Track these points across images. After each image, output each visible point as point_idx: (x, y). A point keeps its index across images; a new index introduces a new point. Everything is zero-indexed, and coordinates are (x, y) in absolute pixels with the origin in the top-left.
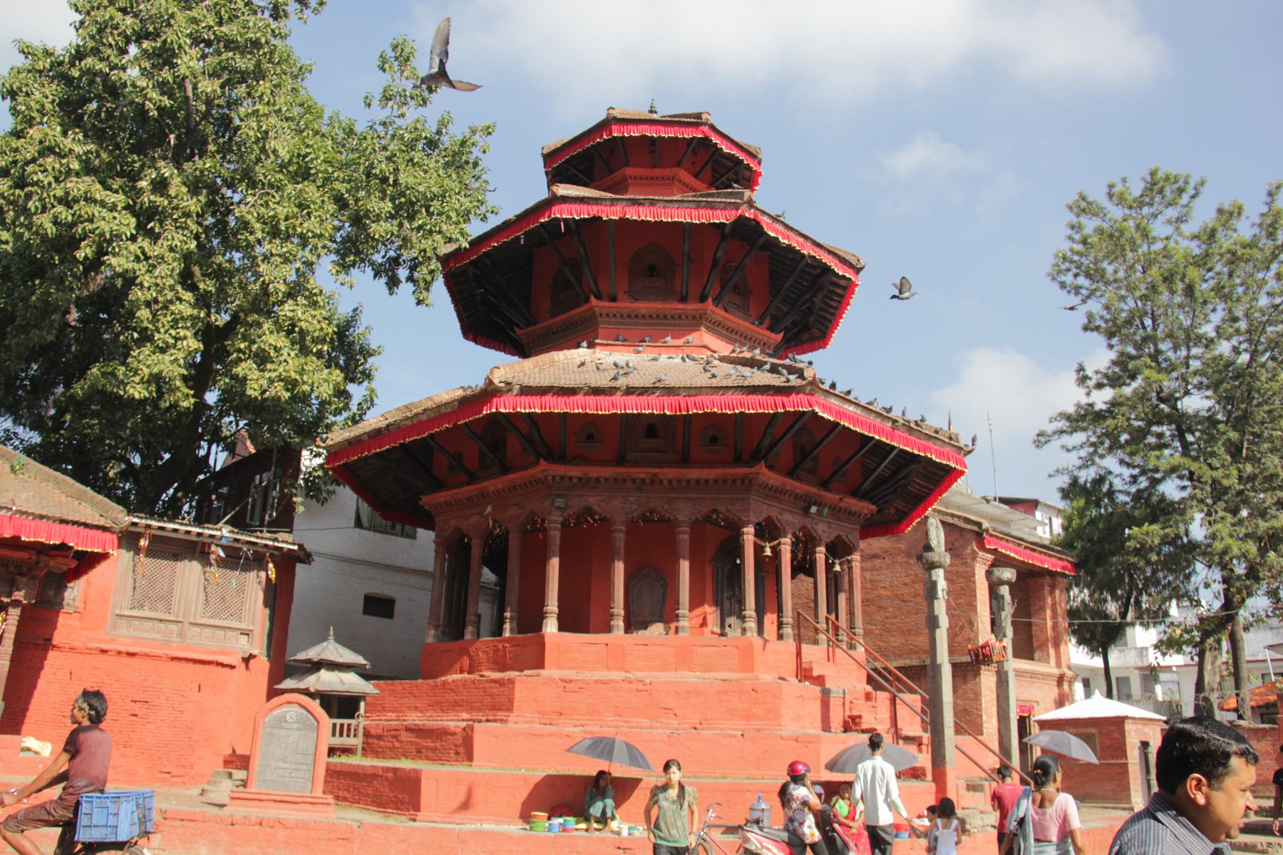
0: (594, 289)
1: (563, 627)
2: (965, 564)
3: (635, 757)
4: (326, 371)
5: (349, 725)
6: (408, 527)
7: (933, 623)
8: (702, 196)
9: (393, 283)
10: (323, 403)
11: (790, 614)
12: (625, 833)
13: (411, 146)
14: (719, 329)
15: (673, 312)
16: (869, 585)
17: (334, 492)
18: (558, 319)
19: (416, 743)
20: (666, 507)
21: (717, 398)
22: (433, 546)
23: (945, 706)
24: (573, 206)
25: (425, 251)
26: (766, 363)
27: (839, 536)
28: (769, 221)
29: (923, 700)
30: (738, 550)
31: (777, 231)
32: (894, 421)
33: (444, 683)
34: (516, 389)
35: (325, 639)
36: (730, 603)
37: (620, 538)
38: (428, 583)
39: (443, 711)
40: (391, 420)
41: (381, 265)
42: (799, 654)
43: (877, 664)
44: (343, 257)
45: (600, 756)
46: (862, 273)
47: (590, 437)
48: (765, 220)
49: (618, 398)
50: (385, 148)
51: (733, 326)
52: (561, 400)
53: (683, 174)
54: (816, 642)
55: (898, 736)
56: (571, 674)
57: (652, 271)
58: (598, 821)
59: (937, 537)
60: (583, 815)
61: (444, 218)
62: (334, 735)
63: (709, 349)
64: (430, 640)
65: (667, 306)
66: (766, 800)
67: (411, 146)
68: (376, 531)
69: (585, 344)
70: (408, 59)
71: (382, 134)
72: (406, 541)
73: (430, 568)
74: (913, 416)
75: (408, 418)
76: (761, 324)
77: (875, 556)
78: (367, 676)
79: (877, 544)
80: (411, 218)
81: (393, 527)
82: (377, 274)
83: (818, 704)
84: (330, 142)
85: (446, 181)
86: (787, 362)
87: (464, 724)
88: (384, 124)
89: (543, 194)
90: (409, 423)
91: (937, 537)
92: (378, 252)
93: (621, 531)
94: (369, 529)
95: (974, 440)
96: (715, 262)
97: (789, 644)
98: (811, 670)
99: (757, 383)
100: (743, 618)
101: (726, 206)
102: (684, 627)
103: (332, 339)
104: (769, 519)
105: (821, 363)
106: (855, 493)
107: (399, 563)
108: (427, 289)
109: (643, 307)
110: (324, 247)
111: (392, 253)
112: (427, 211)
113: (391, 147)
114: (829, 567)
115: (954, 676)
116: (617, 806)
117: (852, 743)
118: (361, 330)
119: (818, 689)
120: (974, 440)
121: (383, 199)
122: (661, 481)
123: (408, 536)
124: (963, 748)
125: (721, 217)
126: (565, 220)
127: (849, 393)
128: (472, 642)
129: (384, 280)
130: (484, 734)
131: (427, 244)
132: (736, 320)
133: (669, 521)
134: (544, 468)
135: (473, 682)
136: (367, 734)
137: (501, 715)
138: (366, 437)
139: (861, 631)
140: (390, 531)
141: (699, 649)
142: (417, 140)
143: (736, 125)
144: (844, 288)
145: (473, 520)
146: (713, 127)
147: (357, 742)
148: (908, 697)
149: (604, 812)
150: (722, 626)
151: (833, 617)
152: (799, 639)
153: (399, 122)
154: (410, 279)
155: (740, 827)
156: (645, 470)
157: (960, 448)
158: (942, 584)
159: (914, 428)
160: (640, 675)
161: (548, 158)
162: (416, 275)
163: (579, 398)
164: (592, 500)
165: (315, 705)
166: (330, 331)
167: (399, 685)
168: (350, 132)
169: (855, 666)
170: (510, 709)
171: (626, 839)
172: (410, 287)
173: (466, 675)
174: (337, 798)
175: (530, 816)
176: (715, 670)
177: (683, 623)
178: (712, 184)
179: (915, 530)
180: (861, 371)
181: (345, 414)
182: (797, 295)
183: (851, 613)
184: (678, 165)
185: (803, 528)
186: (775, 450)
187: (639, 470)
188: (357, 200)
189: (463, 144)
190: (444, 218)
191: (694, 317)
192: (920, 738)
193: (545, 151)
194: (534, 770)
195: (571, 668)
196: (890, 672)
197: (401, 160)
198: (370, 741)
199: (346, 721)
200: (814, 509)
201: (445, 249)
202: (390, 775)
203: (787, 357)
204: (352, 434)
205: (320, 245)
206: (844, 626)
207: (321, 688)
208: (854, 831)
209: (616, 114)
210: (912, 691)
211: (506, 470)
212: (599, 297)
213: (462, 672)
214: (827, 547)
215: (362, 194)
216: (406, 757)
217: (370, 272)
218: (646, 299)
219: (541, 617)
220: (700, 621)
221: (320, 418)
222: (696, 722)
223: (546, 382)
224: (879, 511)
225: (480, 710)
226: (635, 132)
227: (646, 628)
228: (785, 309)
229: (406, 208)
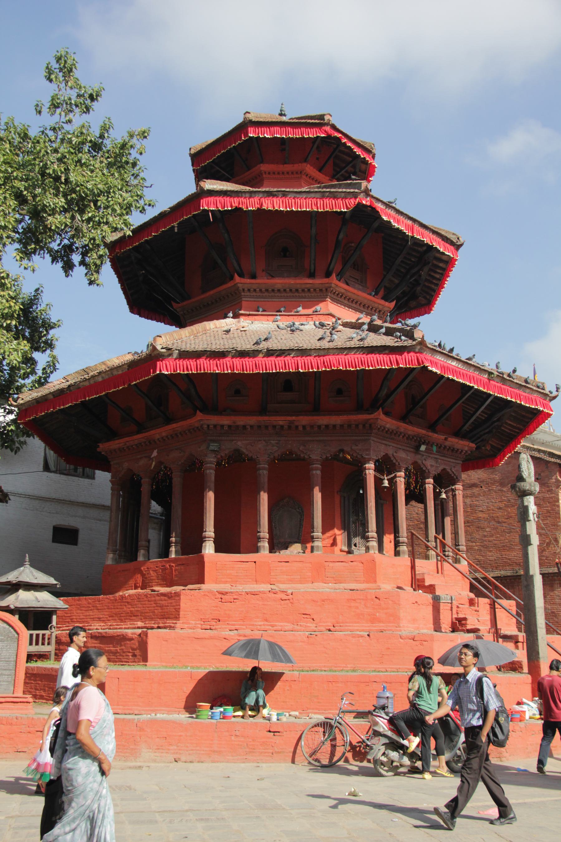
0: (237, 268)
1: (218, 549)
4: (15, 342)
5: (44, 635)
6: (87, 470)
7: (526, 541)
9: (68, 267)
10: (13, 369)
12: (274, 718)
13: (78, 148)
16: (469, 509)
17: (25, 443)
21: (342, 358)
22: (110, 485)
23: (538, 610)
24: (218, 199)
25: (94, 239)
26: (382, 327)
27: (444, 469)
29: (518, 605)
30: (362, 483)
31: (389, 216)
32: (490, 373)
33: (122, 597)
35: (21, 564)
37: (264, 474)
39: (121, 621)
40: (71, 382)
42: (413, 567)
43: (478, 575)
44: (25, 245)
46: (461, 249)
47: (237, 392)
48: (379, 206)
49: (260, 359)
50: (56, 151)
51: (355, 297)
53: (309, 169)
54: (427, 557)
55: (498, 635)
57: (285, 252)
58: (251, 709)
59: (528, 469)
61: (110, 211)
62: (31, 644)
63: (334, 316)
64: (109, 562)
65: (298, 281)
66: (390, 690)
67: (78, 148)
68: (61, 473)
69: (231, 314)
70: (70, 71)
71: (53, 138)
73: (108, 503)
74: (506, 369)
75: (85, 380)
76: (376, 294)
77: (473, 485)
78: (57, 594)
79: (475, 475)
80: (82, 211)
81: (75, 470)
82: (54, 260)
83: (430, 608)
84: (8, 146)
85: (110, 179)
86: (398, 325)
87: (140, 631)
88: (54, 129)
89: (190, 189)
90: (87, 384)
91: (528, 469)
93: (264, 469)
94: (55, 472)
96: (338, 243)
97: (405, 559)
98: (423, 580)
100: (366, 538)
101: (347, 195)
102: (318, 547)
103: (18, 315)
105: (428, 327)
106: (457, 434)
107: (81, 499)
108: (98, 272)
109: (279, 282)
110: (8, 237)
111: (66, 242)
112: (95, 205)
113: (61, 150)
114: (437, 495)
118: (42, 307)
119: (430, 596)
121: (57, 195)
122: (297, 427)
124: (551, 644)
126: (212, 211)
128: (143, 563)
129: (60, 264)
130: (155, 638)
131: (97, 234)
132: (356, 291)
133: (304, 459)
134: (200, 419)
135: (146, 596)
137: (169, 622)
138: (51, 397)
139: (464, 548)
140: (74, 474)
141: (331, 564)
142: (83, 143)
143: (353, 125)
144: (446, 262)
145: (142, 462)
146: (334, 127)
148: (505, 602)
149: (257, 701)
150: (349, 545)
151: (440, 537)
152: (413, 555)
153: (67, 127)
154: (83, 263)
155: (370, 713)
156: (283, 418)
157: (546, 395)
158: (533, 509)
159: (505, 379)
160: (283, 587)
161: (197, 157)
162: (87, 259)
163: (228, 361)
164: (241, 444)
165: (15, 619)
166: (17, 308)
167: (84, 600)
168: (25, 137)
171: (276, 724)
172: (83, 270)
173: (139, 590)
174: (35, 696)
175: (196, 706)
177: (317, 543)
178: (333, 177)
179: (507, 463)
180: (464, 331)
181: (32, 378)
182: (407, 270)
183: (455, 533)
184: (305, 161)
185: (415, 463)
187: (278, 418)
189: (123, 146)
190: (110, 211)
191: (321, 290)
192: (517, 636)
193: (193, 152)
194: (198, 667)
195: (226, 582)
196: (488, 581)
199: (41, 632)
200: (423, 448)
201: (112, 237)
203: (398, 322)
204: (40, 394)
205: (5, 235)
206: (450, 544)
207: (19, 605)
209: (252, 117)
210: (509, 598)
211: (169, 420)
212: (241, 275)
213: (136, 588)
214: (435, 479)
215: (38, 191)
217: (48, 258)
218: (281, 276)
221: (11, 381)
223: (200, 347)
224: (477, 448)
225: (152, 619)
227: (286, 548)
228: (397, 281)
229: (79, 203)
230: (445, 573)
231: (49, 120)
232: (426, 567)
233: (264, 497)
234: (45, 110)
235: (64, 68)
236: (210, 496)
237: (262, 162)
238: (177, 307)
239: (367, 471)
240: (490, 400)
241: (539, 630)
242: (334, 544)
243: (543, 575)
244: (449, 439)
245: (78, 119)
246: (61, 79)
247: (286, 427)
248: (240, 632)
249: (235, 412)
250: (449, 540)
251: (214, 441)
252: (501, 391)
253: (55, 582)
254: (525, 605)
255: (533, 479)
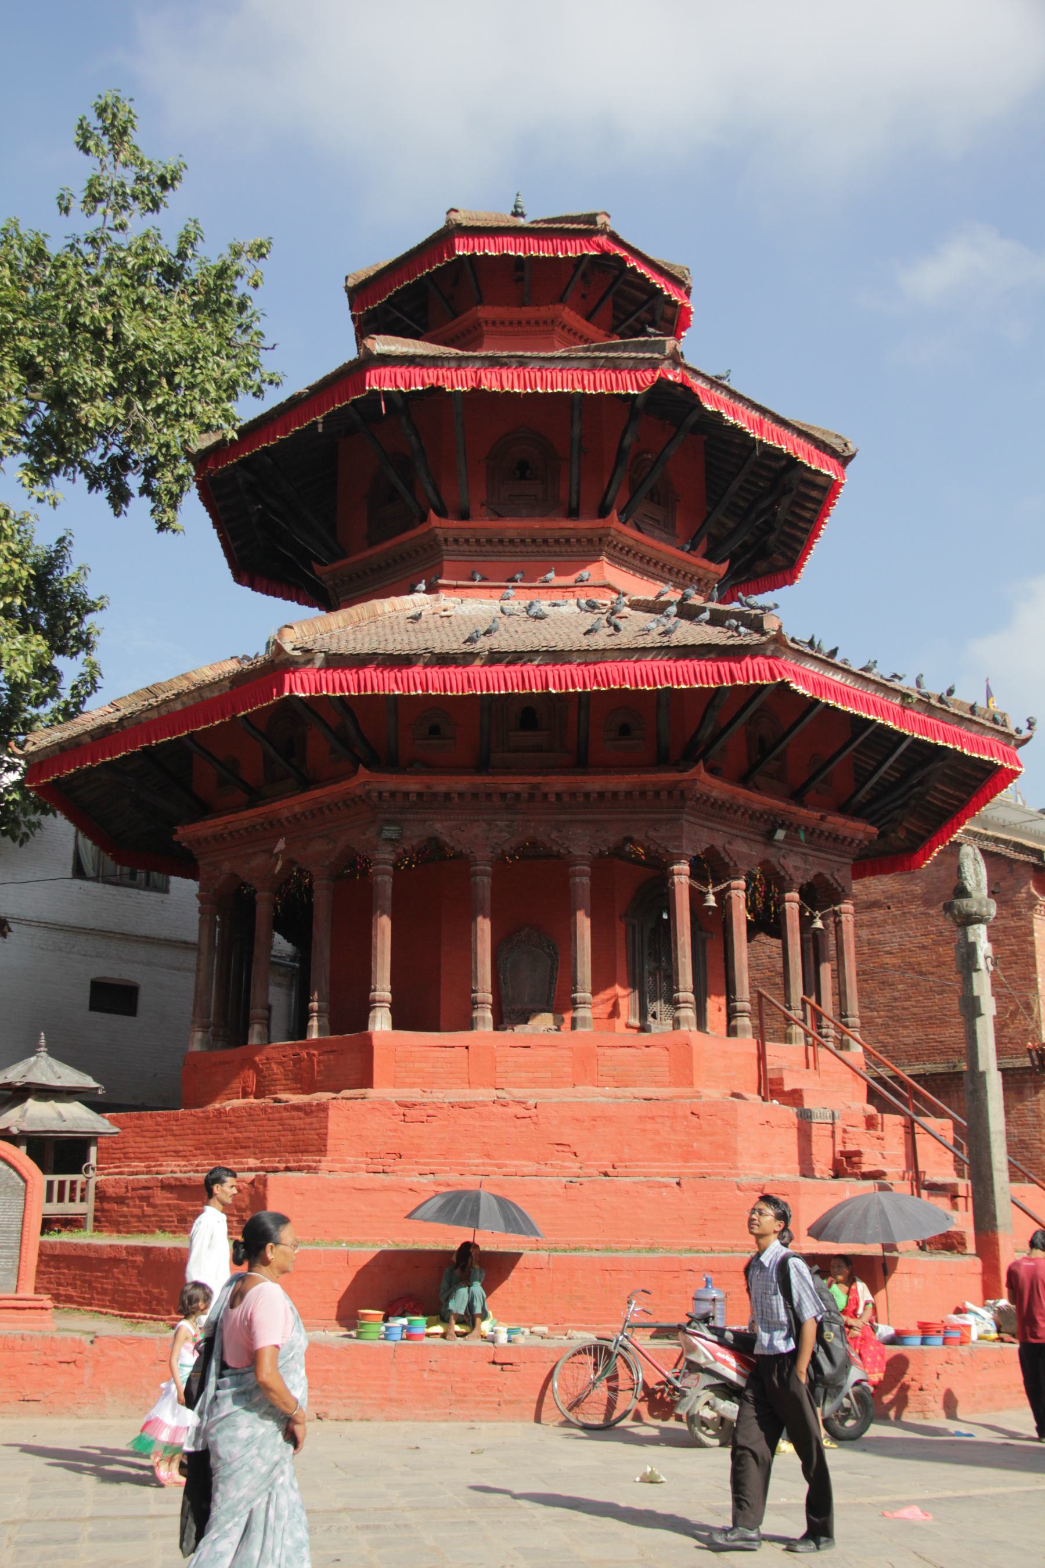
1: (398, 1024)
2: (1017, 914)
3: (513, 1219)
4: (21, 638)
6: (155, 875)
7: (971, 1008)
8: (598, 349)
9: (119, 498)
11: (747, 996)
12: (503, 1338)
13: (139, 277)
14: (630, 558)
15: (557, 534)
16: (866, 950)
17: (39, 825)
18: (378, 549)
19: (177, 1208)
20: (554, 835)
21: (629, 667)
25: (167, 446)
26: (703, 610)
27: (820, 875)
28: (705, 386)
29: (957, 1128)
30: (667, 900)
31: (717, 402)
32: (905, 696)
33: (220, 1112)
34: (319, 662)
35: (33, 1052)
36: (653, 982)
37: (484, 883)
38: (190, 959)
40: (125, 711)
41: (99, 469)
42: (761, 1057)
43: (883, 1072)
44: (39, 457)
45: (458, 1222)
46: (851, 465)
47: (435, 731)
48: (698, 384)
49: (476, 670)
50: (97, 282)
51: (652, 553)
52: (389, 675)
53: (568, 315)
54: (787, 1039)
56: (413, 1094)
57: (523, 471)
59: (975, 874)
60: (438, 1312)
61: (197, 393)
62: (49, 1199)
64: (196, 1047)
65: (549, 524)
66: (717, 1286)
67: (139, 277)
68: (106, 882)
69: (422, 586)
70: (124, 132)
71: (91, 258)
72: (153, 896)
73: (193, 936)
74: (934, 688)
75: (152, 708)
76: (693, 548)
78: (97, 1106)
79: (877, 885)
80: (145, 394)
81: (133, 876)
82: (93, 484)
83: (794, 1133)
85: (198, 334)
86: (735, 606)
87: (252, 1175)
88: (92, 241)
89: (349, 353)
90: (154, 715)
91: (975, 874)
92: (94, 449)
93: (484, 873)
94: (95, 879)
95: (1031, 725)
97: (746, 1043)
98: (780, 1081)
99: (690, 641)
100: (674, 1003)
101: (638, 365)
102: (584, 1019)
103: (27, 587)
104: (711, 851)
105: (788, 609)
106: (844, 809)
107: (144, 930)
108: (174, 507)
109: (511, 526)
111: (115, 450)
112: (170, 382)
113: (107, 280)
114: (805, 923)
115: (1006, 1089)
116: (489, 1289)
117: (847, 1195)
118: (71, 572)
119: (792, 1111)
120: (1031, 725)
121: (98, 365)
122: (545, 795)
123: (156, 889)
125: (631, 385)
127: (833, 653)
128: (259, 1049)
129: (104, 493)
131: (172, 436)
132: (654, 543)
133: (558, 856)
134: (365, 780)
135: (264, 1110)
136: (101, 1196)
137: (308, 1159)
138: (87, 739)
140: (129, 882)
142: (147, 267)
143: (650, 233)
144: (823, 489)
145: (258, 861)
146: (614, 237)
147: (86, 1208)
148: (932, 1122)
149: (470, 1306)
150: (643, 1014)
151: (813, 1000)
152: (761, 1035)
153: (117, 237)
154: (146, 490)
155: (680, 1328)
156: (519, 779)
157: (1009, 736)
158: (984, 948)
160: (519, 1093)
161: (359, 294)
163: (416, 672)
164: (440, 827)
165: (19, 1154)
166: (24, 574)
168: (39, 255)
169: (849, 1074)
170: (321, 1150)
171: (505, 1348)
173: (252, 1100)
174: (56, 1298)
175: (357, 1316)
176: (634, 1085)
178: (612, 331)
179: (937, 863)
180: (848, 616)
181: (52, 704)
182: (752, 504)
183: (841, 994)
184: (561, 300)
185: (765, 864)
186: (718, 746)
187: (510, 779)
188: (57, 367)
189: (222, 272)
190: (197, 393)
191: (590, 541)
192: (954, 1186)
193: (351, 283)
194: (361, 1244)
195: (412, 1085)
196: (902, 1083)
197: (123, 300)
198: (106, 1206)
199: (68, 1178)
200: (780, 834)
201: (202, 442)
202: (139, 1258)
203: (734, 599)
204: (66, 735)
208: (856, 1333)
209: (462, 218)
210: (940, 1114)
211: (306, 783)
212: (441, 513)
213: (245, 1095)
215: (64, 356)
216: (163, 1230)
217: (82, 481)
219: (366, 1007)
220: (608, 1008)
222: (606, 1165)
224: (880, 836)
225: (275, 1153)
226: (490, 249)
227: (525, 1021)
229: (136, 379)
230: (821, 1067)
231: (83, 224)
232: (784, 1057)
233: (484, 927)
234: (76, 206)
235: (111, 127)
236: (384, 926)
237: (480, 302)
238: (322, 572)
239: (676, 879)
240: (904, 745)
241: (996, 1174)
242: (614, 1013)
243: (1004, 1072)
244: (830, 818)
245: (138, 223)
246: (107, 147)
247: (525, 795)
248: (440, 1177)
249: (430, 767)
250: (828, 1006)
251: (389, 822)
252: (925, 729)
253: (94, 1085)
254: (971, 1127)
255: (985, 892)
